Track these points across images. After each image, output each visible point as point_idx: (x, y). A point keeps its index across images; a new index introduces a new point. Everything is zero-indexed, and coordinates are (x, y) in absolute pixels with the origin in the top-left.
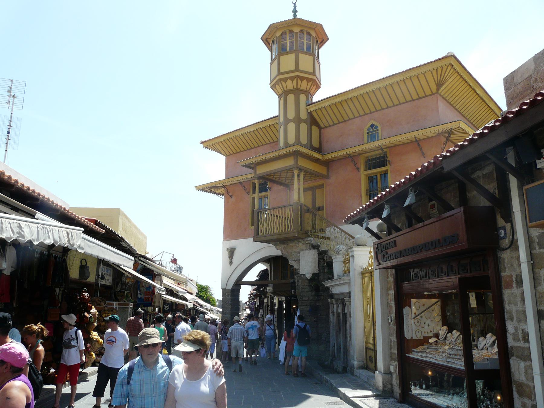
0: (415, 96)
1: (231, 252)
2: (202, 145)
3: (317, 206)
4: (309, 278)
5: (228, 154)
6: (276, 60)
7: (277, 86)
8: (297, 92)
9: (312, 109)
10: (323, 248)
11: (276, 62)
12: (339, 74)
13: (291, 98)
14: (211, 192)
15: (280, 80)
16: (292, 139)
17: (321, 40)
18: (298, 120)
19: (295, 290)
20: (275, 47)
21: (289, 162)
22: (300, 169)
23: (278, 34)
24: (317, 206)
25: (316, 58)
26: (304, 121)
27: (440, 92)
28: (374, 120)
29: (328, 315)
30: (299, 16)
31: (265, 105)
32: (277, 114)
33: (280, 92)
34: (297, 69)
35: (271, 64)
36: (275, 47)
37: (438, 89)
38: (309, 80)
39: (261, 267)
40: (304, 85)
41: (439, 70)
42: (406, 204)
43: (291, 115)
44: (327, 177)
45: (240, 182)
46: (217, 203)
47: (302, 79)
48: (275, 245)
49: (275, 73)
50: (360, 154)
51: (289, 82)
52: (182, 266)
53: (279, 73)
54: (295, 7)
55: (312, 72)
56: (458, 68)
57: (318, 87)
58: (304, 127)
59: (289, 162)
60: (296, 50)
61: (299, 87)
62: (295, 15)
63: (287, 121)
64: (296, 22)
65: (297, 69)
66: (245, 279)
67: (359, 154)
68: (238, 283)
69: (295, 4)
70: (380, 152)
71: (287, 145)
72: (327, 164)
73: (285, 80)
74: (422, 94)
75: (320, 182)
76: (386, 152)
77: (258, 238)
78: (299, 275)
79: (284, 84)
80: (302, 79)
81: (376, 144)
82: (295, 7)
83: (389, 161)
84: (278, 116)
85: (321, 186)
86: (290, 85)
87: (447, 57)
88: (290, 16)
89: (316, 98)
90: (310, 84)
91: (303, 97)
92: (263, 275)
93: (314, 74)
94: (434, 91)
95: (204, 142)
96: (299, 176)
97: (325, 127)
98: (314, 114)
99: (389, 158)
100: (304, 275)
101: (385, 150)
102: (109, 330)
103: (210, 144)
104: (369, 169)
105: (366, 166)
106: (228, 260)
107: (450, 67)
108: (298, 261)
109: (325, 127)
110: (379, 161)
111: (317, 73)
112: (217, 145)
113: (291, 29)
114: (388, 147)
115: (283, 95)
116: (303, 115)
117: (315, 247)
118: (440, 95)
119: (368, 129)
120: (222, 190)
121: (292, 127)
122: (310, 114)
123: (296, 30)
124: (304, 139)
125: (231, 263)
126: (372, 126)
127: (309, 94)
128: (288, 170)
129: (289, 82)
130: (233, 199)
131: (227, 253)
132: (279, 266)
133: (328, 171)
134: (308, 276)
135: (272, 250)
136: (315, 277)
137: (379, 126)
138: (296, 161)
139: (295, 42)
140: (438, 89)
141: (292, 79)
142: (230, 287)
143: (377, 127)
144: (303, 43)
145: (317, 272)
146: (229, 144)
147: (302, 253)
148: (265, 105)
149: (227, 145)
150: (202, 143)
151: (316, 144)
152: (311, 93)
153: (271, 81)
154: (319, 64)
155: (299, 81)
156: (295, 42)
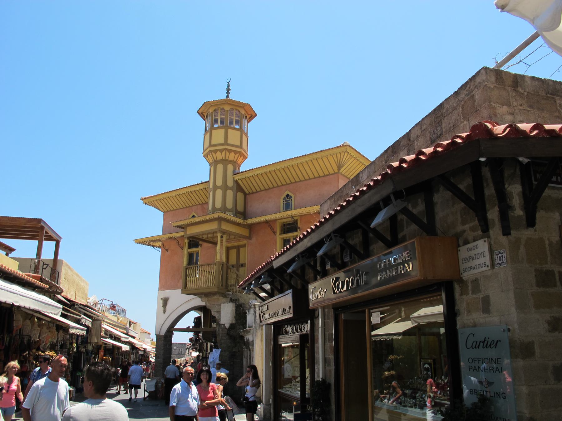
0: (322, 174)
1: (165, 301)
2: (142, 202)
3: (241, 263)
4: (227, 328)
5: (166, 211)
6: (209, 131)
7: (209, 156)
8: (225, 162)
9: (238, 177)
10: (241, 301)
11: (208, 134)
12: (265, 149)
13: (220, 167)
14: (149, 245)
15: (211, 151)
16: (219, 204)
17: (250, 116)
18: (225, 188)
19: (216, 337)
20: (209, 120)
21: (213, 226)
22: (224, 232)
23: (211, 110)
24: (241, 263)
25: (243, 133)
26: (230, 188)
27: (341, 171)
28: (289, 191)
29: (242, 360)
30: (231, 97)
31: (199, 172)
32: (208, 180)
33: (211, 161)
34: (226, 143)
35: (205, 135)
36: (209, 120)
37: (339, 170)
38: (236, 152)
39: (195, 314)
40: (232, 157)
41: (339, 155)
42: (473, 198)
43: (219, 182)
44: (249, 238)
45: (175, 238)
46: (154, 255)
47: (230, 151)
48: (200, 297)
49: (207, 144)
50: (276, 220)
51: (219, 153)
52: (125, 308)
53: (211, 145)
54: (229, 86)
55: (239, 144)
56: (354, 154)
57: (245, 158)
58: (230, 193)
59: (213, 226)
60: (226, 124)
61: (227, 158)
62: (228, 96)
63: (216, 188)
64: (227, 101)
65: (226, 143)
66: (176, 327)
67: (275, 221)
68: (171, 330)
69: (228, 83)
70: (290, 219)
71: (215, 210)
72: (251, 227)
73: (215, 151)
74: (327, 173)
75: (244, 242)
76: (297, 220)
77: (186, 290)
78: (218, 324)
79: (214, 154)
80: (230, 151)
81: (289, 213)
82: (229, 86)
83: (299, 228)
84: (207, 182)
85: (244, 246)
86: (219, 156)
87: (343, 146)
88: (224, 97)
89: (242, 169)
90: (237, 155)
91: (230, 168)
92: (197, 321)
93: (241, 147)
94: (336, 171)
95: (144, 199)
96: (222, 237)
97: (250, 194)
98: (240, 182)
99: (299, 225)
100: (224, 325)
101: (295, 218)
102: (41, 382)
103: (148, 201)
104: (284, 233)
105: (281, 231)
106: (162, 309)
107: (346, 154)
108: (219, 312)
109: (250, 194)
110: (290, 227)
111: (244, 146)
112: (155, 202)
113: (222, 107)
114: (299, 216)
115: (214, 164)
116: (230, 183)
117: (232, 300)
118: (341, 174)
119: (284, 198)
120: (159, 244)
121: (219, 193)
122: (236, 182)
123: (227, 108)
124: (230, 205)
125: (164, 311)
126: (287, 196)
127: (236, 164)
128: (214, 233)
129: (219, 153)
130: (168, 253)
131: (161, 302)
132: (207, 317)
133: (250, 233)
134: (227, 326)
135: (198, 302)
136: (232, 326)
137: (293, 196)
138: (220, 225)
139: (227, 117)
140: (339, 170)
141: (221, 151)
142: (163, 333)
143: (291, 197)
144: (233, 119)
145: (234, 322)
146: (167, 202)
147: (222, 305)
148: (199, 172)
149: (167, 203)
150: (142, 199)
151: (240, 208)
152: (239, 162)
153: (204, 151)
154: (247, 137)
155: (228, 153)
156: (227, 117)
